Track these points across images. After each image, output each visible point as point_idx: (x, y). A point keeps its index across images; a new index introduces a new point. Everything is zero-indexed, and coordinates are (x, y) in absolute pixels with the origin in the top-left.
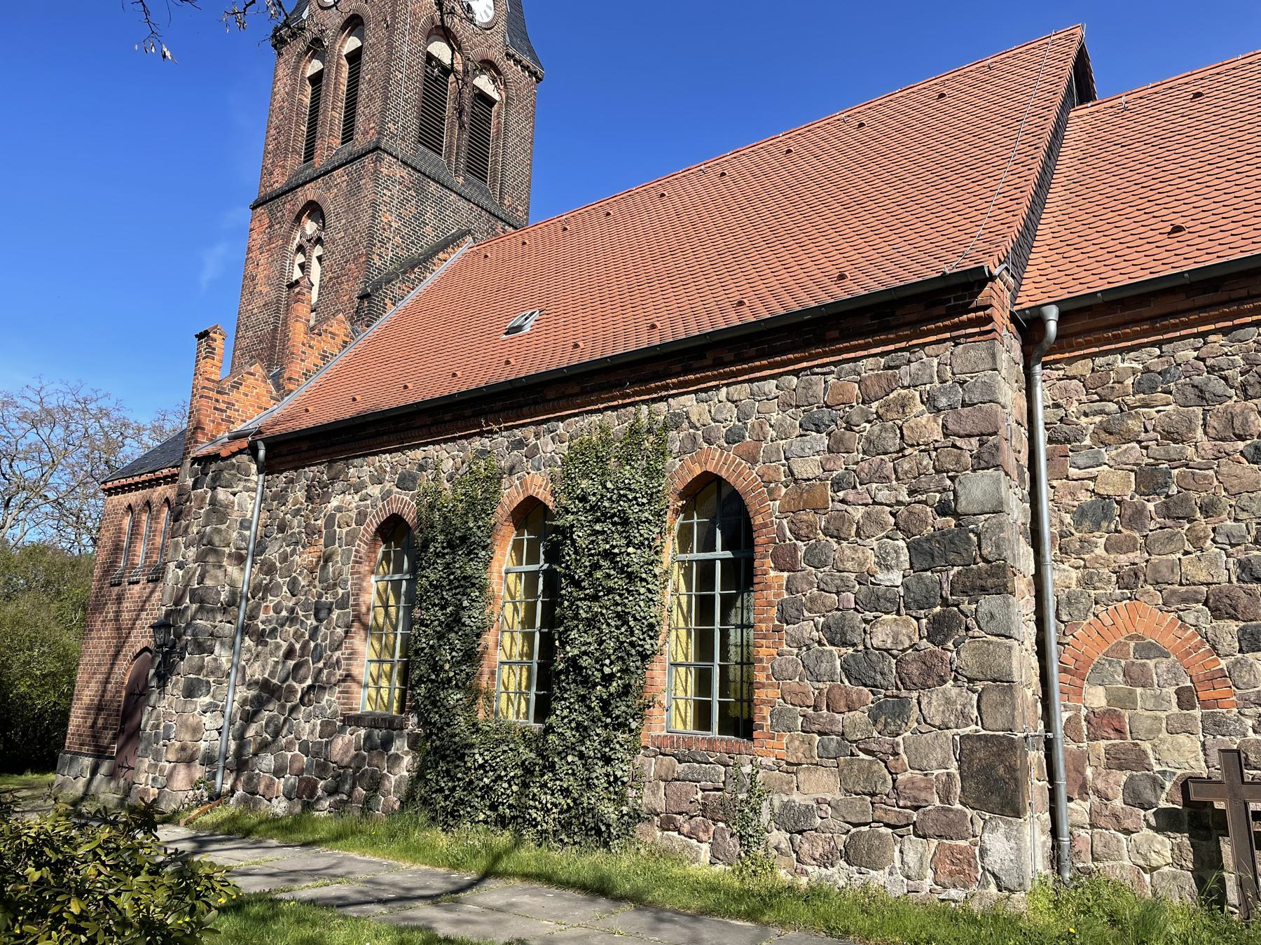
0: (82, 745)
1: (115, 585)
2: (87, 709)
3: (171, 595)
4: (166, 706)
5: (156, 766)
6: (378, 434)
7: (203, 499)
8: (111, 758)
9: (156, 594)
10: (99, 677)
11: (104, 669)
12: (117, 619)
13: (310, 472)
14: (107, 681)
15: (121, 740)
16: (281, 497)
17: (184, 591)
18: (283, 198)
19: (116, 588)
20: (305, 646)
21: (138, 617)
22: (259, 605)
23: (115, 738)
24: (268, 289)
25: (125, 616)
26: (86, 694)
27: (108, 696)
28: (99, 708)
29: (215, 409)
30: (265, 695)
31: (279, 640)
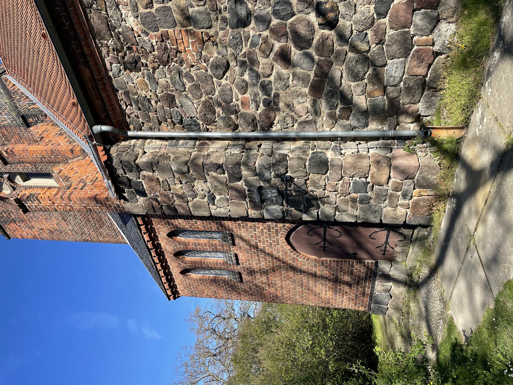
0: (364, 294)
1: (241, 277)
2: (336, 292)
4: (337, 200)
5: (391, 195)
7: (151, 179)
8: (376, 264)
10: (311, 283)
11: (305, 279)
12: (265, 272)
14: (314, 275)
15: (362, 255)
19: (244, 276)
20: (278, 33)
21: (263, 251)
23: (360, 261)
24: (53, 218)
25: (263, 265)
26: (325, 294)
27: (326, 273)
28: (336, 281)
29: (82, 189)
30: (327, 88)
31: (272, 78)
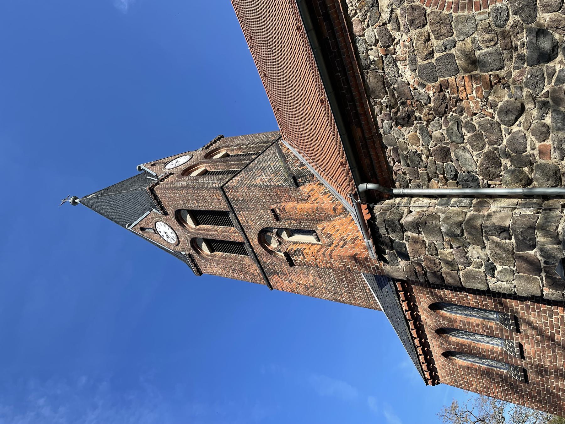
1: (526, 376)
3: (527, 280)
6: (327, 17)
7: (415, 241)
9: (533, 320)
13: (383, 123)
16: (413, 160)
17: (521, 258)
18: (265, 270)
19: (530, 376)
22: (542, 168)
29: (342, 247)
